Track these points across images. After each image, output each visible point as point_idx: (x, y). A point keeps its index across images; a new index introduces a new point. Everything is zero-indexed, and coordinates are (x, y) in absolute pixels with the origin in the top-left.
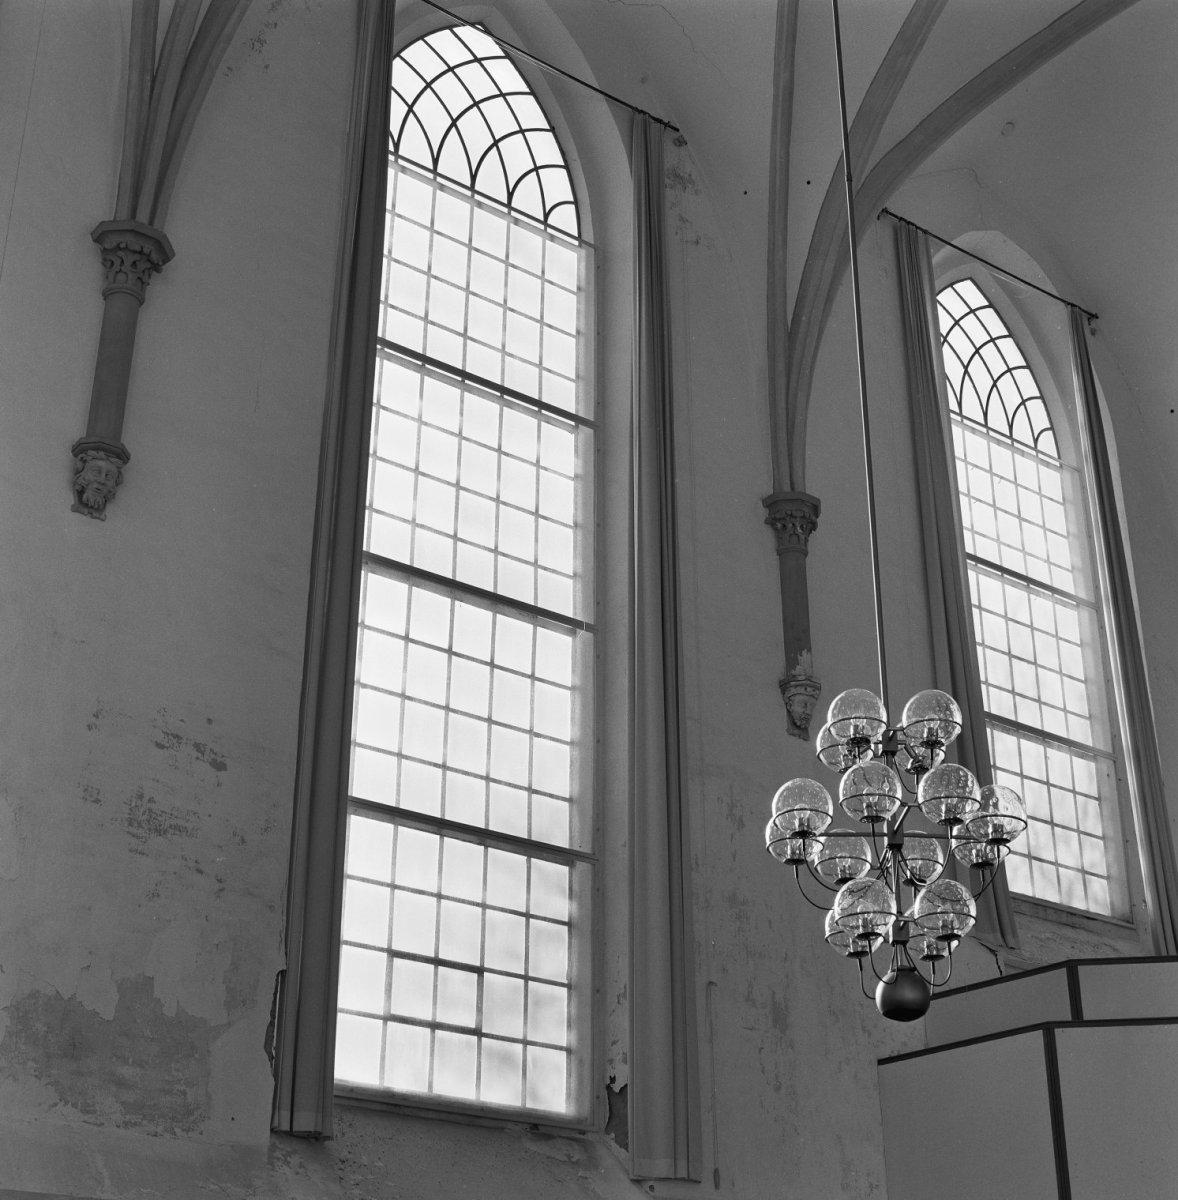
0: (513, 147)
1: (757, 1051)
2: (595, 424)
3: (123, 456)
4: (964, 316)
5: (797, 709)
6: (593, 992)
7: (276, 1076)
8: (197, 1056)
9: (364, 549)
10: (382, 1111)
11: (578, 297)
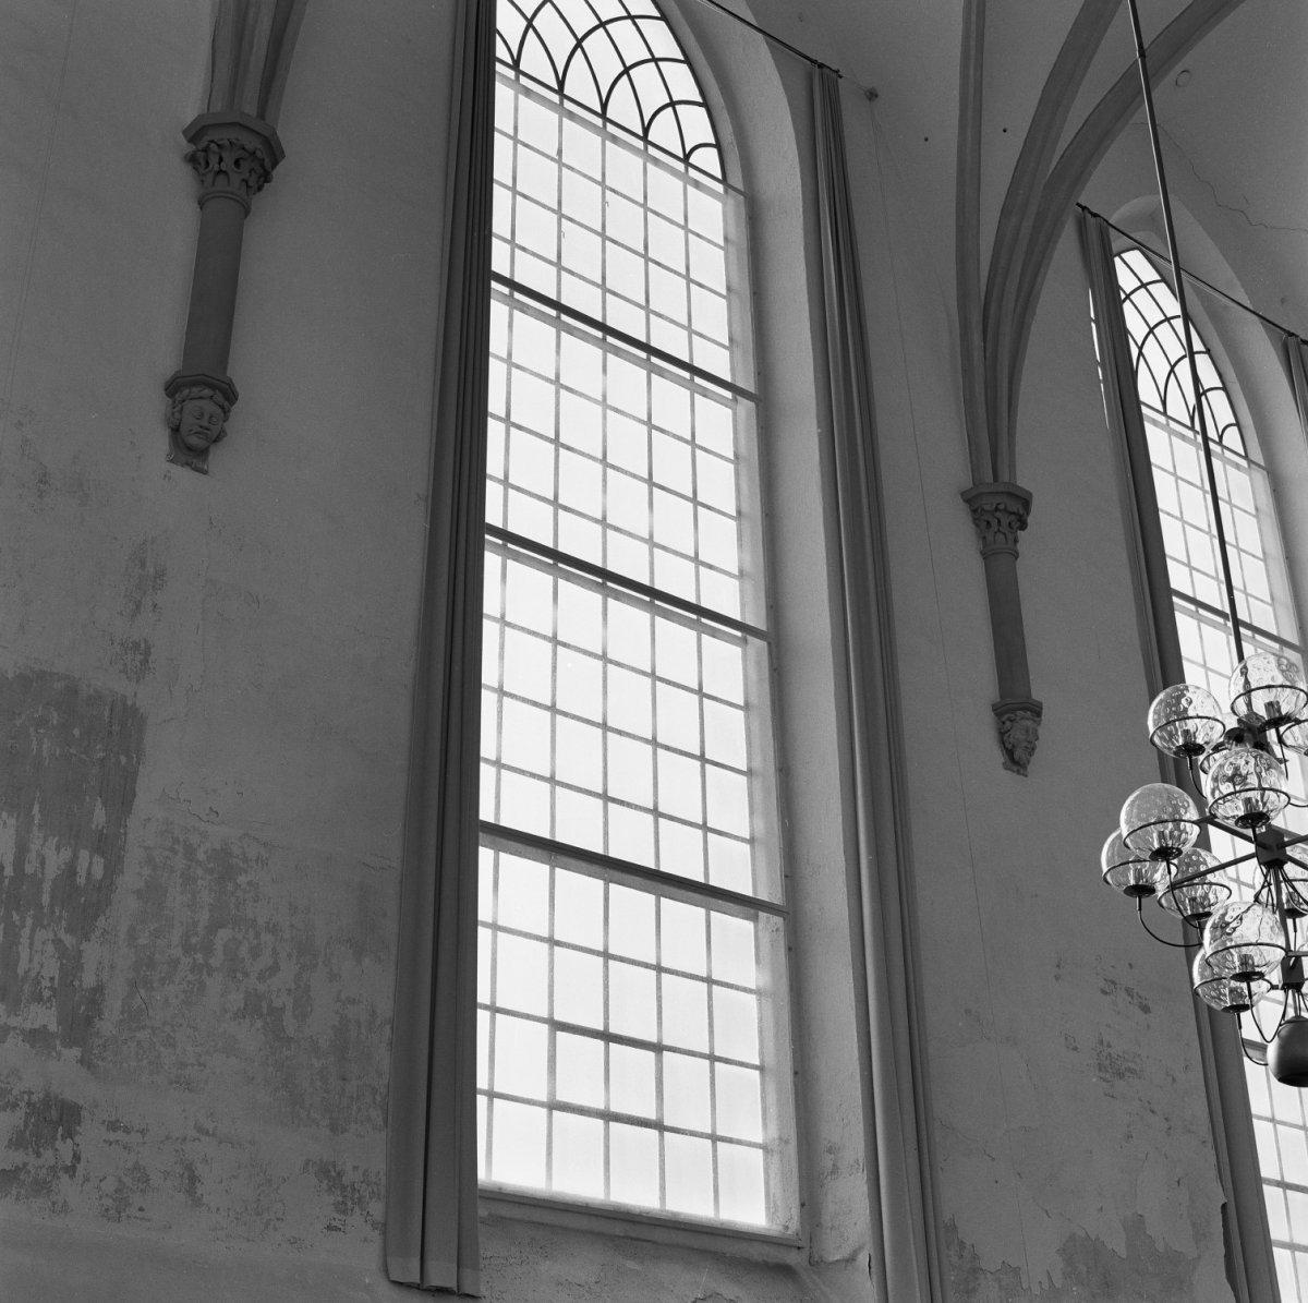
0: (645, 76)
2: (785, 913)
3: (229, 395)
4: (1132, 269)
9: (482, 1175)
11: (724, 205)
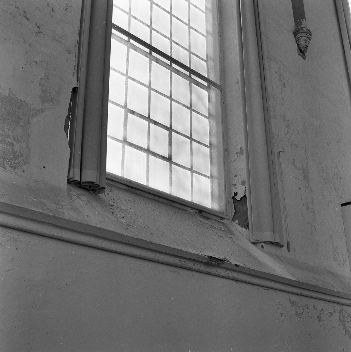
1: (299, 189)
5: (302, 43)
6: (224, 153)
7: (71, 145)
8: (21, 124)
10: (124, 189)
